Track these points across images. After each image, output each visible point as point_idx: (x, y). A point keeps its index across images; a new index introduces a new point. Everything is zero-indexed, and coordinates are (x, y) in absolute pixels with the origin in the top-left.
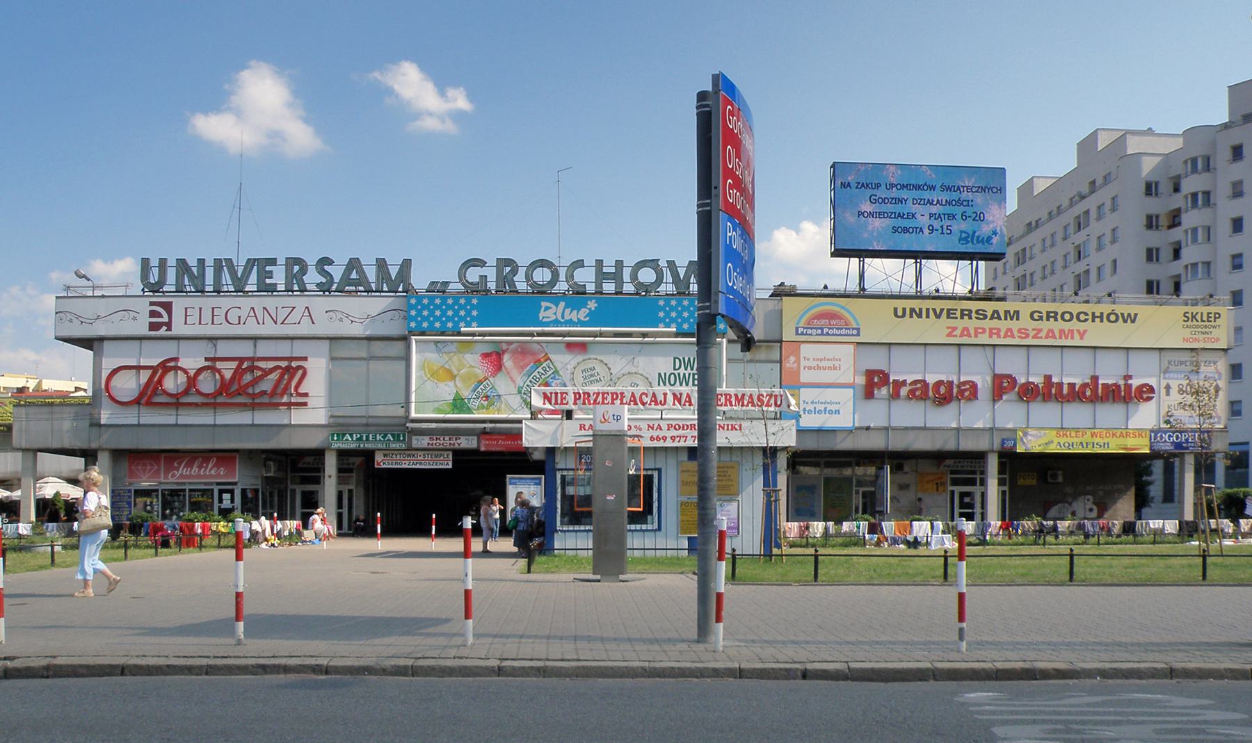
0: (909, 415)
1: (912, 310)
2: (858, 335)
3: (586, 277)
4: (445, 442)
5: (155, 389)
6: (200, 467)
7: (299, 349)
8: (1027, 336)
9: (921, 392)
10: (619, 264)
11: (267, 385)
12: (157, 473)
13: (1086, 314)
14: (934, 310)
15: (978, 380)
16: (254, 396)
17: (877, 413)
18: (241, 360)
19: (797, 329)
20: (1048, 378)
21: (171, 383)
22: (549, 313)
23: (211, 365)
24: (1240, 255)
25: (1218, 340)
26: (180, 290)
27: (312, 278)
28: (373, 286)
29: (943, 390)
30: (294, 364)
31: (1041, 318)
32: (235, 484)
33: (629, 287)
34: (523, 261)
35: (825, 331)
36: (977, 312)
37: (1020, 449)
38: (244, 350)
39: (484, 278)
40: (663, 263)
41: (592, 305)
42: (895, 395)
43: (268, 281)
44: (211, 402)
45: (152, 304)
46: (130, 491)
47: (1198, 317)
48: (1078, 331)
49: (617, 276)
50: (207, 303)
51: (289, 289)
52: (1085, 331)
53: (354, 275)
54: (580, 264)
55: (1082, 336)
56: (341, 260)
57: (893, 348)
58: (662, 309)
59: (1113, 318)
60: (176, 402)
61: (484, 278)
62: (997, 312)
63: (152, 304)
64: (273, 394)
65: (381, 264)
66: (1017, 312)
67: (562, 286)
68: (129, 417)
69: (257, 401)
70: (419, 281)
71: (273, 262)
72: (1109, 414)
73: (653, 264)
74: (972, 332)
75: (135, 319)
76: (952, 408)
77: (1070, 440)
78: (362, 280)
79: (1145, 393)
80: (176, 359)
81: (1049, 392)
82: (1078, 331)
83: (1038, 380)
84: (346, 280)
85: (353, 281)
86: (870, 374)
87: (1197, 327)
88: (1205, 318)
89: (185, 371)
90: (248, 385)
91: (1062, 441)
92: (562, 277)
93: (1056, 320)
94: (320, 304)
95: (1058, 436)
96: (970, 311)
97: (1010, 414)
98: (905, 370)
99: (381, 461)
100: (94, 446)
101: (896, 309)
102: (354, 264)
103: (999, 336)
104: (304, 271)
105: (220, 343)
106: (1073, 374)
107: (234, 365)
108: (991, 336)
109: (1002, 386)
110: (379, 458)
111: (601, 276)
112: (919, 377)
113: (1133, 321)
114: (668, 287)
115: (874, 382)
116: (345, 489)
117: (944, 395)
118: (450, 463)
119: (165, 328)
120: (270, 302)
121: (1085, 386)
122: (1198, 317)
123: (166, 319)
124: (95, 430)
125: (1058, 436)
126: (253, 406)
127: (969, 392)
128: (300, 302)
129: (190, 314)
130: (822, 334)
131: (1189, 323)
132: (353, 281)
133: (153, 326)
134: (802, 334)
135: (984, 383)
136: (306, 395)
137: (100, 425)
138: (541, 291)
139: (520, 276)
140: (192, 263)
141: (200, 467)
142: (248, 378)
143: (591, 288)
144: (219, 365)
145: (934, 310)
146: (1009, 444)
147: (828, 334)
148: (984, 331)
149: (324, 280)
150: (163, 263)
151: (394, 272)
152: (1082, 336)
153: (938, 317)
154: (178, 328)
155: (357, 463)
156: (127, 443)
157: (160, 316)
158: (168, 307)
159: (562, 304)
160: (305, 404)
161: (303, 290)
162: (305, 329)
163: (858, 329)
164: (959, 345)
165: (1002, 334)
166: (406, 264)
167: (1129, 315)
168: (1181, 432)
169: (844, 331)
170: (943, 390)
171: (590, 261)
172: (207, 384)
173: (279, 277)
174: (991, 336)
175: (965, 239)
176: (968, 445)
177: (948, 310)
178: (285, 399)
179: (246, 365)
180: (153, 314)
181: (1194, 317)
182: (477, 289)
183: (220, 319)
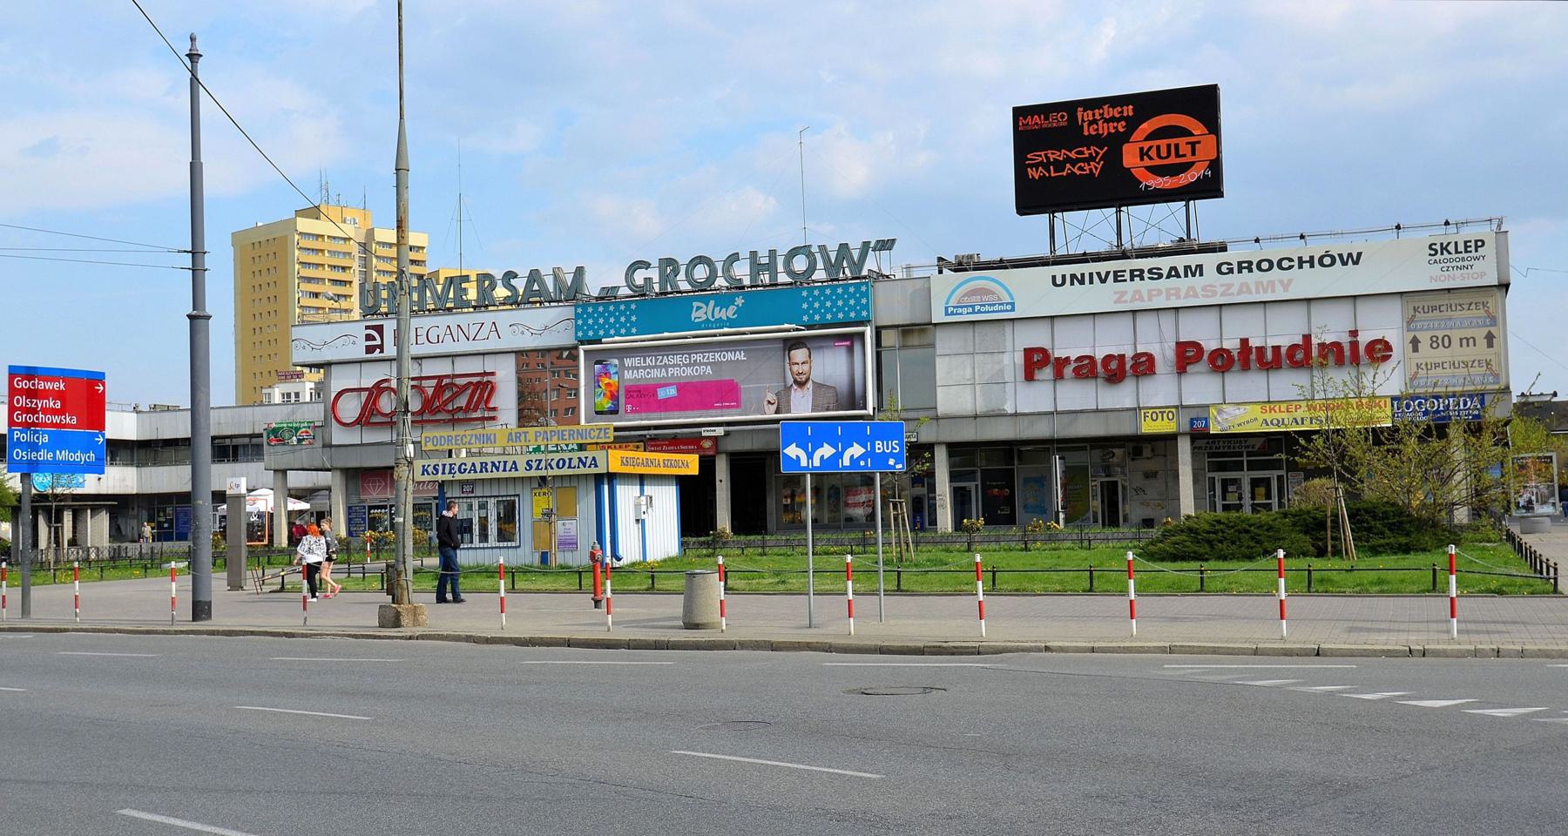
0: (1077, 395)
1: (1073, 276)
2: (1013, 310)
3: (742, 271)
5: (372, 410)
7: (489, 365)
8: (1214, 294)
9: (1086, 369)
11: (462, 401)
13: (1291, 260)
14: (1099, 274)
15: (1154, 350)
18: (440, 378)
20: (1245, 342)
22: (701, 313)
25: (1483, 274)
27: (501, 292)
29: (1113, 365)
31: (1231, 271)
33: (783, 278)
34: (683, 260)
36: (1150, 271)
38: (442, 368)
39: (648, 280)
40: (815, 249)
41: (739, 301)
42: (1059, 376)
45: (367, 328)
47: (1451, 248)
48: (1281, 282)
49: (771, 267)
52: (1290, 281)
53: (536, 287)
54: (734, 257)
55: (1286, 287)
56: (524, 272)
57: (1058, 324)
58: (805, 300)
59: (1327, 261)
62: (1174, 268)
63: (367, 328)
64: (467, 409)
65: (556, 275)
66: (1200, 267)
67: (721, 282)
68: (352, 437)
70: (593, 287)
71: (466, 279)
72: (1338, 380)
73: (805, 250)
74: (1145, 296)
77: (1279, 416)
79: (1379, 351)
81: (1248, 358)
82: (1281, 282)
83: (1232, 344)
85: (533, 295)
86: (1029, 353)
87: (1449, 260)
88: (1461, 248)
90: (446, 403)
91: (1268, 417)
93: (1251, 271)
94: (505, 317)
95: (1264, 411)
96: (1142, 271)
97: (1201, 388)
98: (1070, 345)
101: (1054, 277)
102: (534, 276)
103: (1178, 297)
104: (493, 286)
106: (1282, 332)
108: (1168, 298)
109: (1187, 355)
111: (756, 267)
112: (1087, 352)
113: (1356, 263)
114: (820, 274)
115: (1035, 361)
117: (1114, 371)
121: (1294, 347)
122: (1451, 248)
123: (378, 342)
125: (1264, 411)
127: (1144, 366)
131: (1438, 256)
132: (533, 295)
133: (370, 350)
135: (1164, 353)
136: (494, 409)
137: (331, 446)
138: (702, 288)
142: (447, 394)
143: (747, 282)
144: (425, 383)
145: (1099, 274)
146: (1200, 425)
147: (979, 312)
148: (1160, 292)
151: (569, 279)
152: (1286, 287)
153: (1103, 281)
158: (379, 329)
159: (712, 303)
160: (493, 418)
163: (1013, 304)
164: (1134, 312)
165: (1183, 293)
166: (580, 271)
167: (1350, 255)
168: (1437, 398)
169: (996, 308)
170: (1113, 365)
171: (745, 254)
174: (1168, 298)
176: (1149, 427)
178: (478, 414)
179: (443, 385)
180: (369, 337)
181: (1444, 248)
182: (641, 292)
183: (422, 339)
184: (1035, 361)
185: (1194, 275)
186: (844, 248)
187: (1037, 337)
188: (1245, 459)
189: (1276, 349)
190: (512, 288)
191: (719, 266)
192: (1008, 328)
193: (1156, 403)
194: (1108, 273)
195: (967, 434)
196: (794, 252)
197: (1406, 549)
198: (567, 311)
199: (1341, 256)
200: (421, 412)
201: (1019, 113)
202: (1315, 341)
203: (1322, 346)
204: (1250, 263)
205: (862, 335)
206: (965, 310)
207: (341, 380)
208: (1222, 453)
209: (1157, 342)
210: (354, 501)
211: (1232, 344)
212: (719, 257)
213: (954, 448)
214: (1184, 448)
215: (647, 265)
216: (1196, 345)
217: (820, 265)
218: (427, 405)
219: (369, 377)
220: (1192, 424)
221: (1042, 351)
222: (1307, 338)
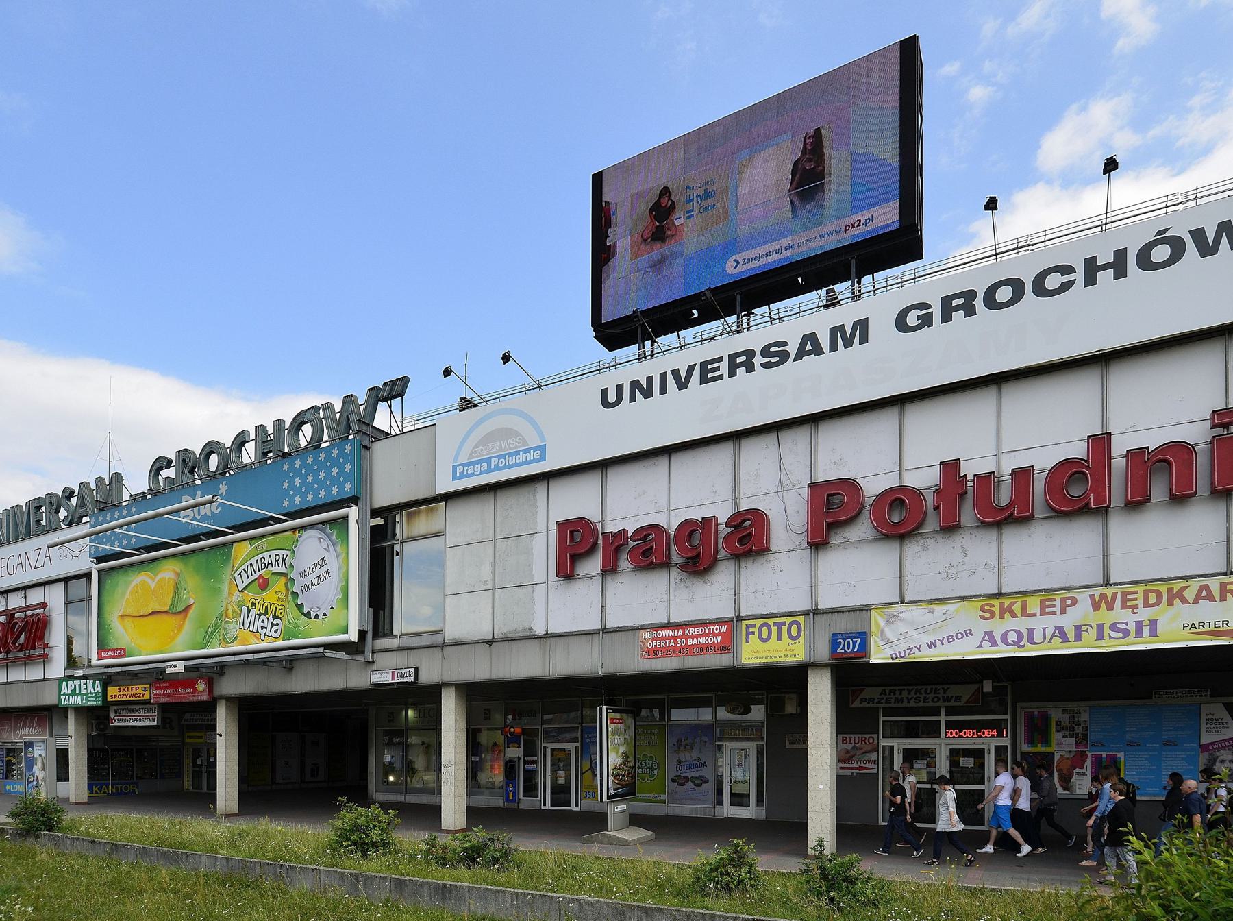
1: (635, 385)
2: (543, 458)
7: (35, 597)
9: (648, 550)
13: (1066, 269)
14: (676, 373)
15: (771, 508)
17: (576, 606)
19: (454, 468)
20: (949, 468)
24: (59, 779)
31: (926, 321)
35: (494, 462)
37: (878, 655)
42: (609, 570)
76: (723, 576)
77: (1023, 624)
83: (924, 478)
96: (750, 354)
97: (857, 572)
98: (627, 506)
101: (605, 392)
105: (30, 593)
109: (832, 509)
127: (747, 537)
130: (489, 470)
134: (462, 476)
135: (787, 516)
146: (849, 647)
147: (497, 468)
153: (682, 385)
163: (542, 448)
169: (520, 458)
176: (756, 652)
177: (704, 365)
184: (577, 545)
185: (848, 343)
187: (575, 501)
188: (943, 718)
189: (1023, 475)
192: (541, 489)
193: (769, 609)
194: (691, 369)
195: (480, 669)
197: (742, 805)
199: (1198, 235)
202: (1119, 447)
203: (1136, 455)
204: (970, 295)
206: (477, 469)
208: (882, 695)
209: (774, 485)
211: (924, 478)
213: (472, 692)
214: (820, 696)
215: (169, 464)
216: (850, 486)
220: (834, 644)
221: (583, 523)
222: (1100, 442)
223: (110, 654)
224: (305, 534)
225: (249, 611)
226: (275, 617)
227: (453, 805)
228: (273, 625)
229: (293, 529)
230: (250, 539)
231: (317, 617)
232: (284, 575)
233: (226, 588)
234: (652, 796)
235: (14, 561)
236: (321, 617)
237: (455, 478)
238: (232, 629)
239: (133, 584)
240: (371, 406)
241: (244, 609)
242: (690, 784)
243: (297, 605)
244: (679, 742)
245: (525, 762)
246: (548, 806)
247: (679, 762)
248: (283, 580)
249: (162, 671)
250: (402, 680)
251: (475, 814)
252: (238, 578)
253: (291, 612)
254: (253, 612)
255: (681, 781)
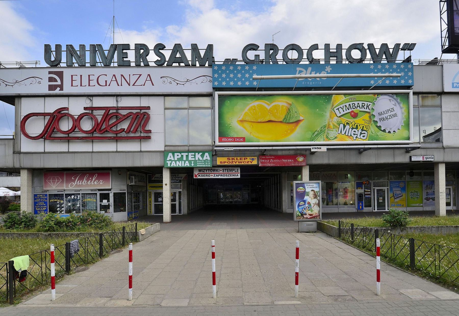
3: (319, 55)
4: (237, 161)
6: (88, 181)
7: (144, 102)
10: (339, 47)
12: (63, 182)
16: (117, 132)
18: (107, 109)
19: (453, 84)
21: (65, 125)
23: (90, 112)
26: (70, 65)
27: (152, 57)
28: (190, 63)
30: (143, 111)
32: (110, 190)
34: (281, 46)
38: (110, 103)
39: (257, 56)
43: (125, 59)
44: (90, 137)
45: (50, 73)
46: (46, 195)
50: (85, 72)
51: (138, 65)
53: (178, 55)
54: (315, 47)
56: (170, 46)
60: (68, 138)
61: (257, 56)
63: (50, 73)
64: (128, 131)
65: (195, 48)
68: (38, 146)
69: (119, 135)
71: (127, 47)
75: (40, 83)
78: (183, 59)
80: (67, 109)
84: (173, 59)
89: (72, 117)
92: (305, 56)
99: (197, 175)
100: (17, 166)
102: (178, 48)
105: (95, 99)
107: (102, 112)
110: (196, 172)
116: (177, 191)
118: (239, 175)
119: (58, 89)
120: (125, 71)
123: (59, 83)
124: (17, 156)
126: (117, 139)
128: (144, 71)
129: (75, 79)
133: (51, 88)
137: (20, 153)
139: (279, 56)
140: (77, 48)
141: (88, 181)
144: (95, 112)
149: (159, 59)
150: (58, 47)
151: (202, 53)
154: (67, 89)
155: (182, 175)
156: (38, 163)
157: (56, 81)
158: (60, 75)
161: (147, 65)
162: (148, 89)
166: (210, 47)
171: (321, 46)
172: (87, 125)
173: (131, 56)
175: (233, 170)
178: (138, 135)
180: (51, 79)
183: (94, 83)
186: (384, 46)
190: (162, 56)
191: (305, 52)
196: (354, 46)
198: (207, 71)
200: (92, 132)
201: (341, 45)
205: (408, 94)
207: (27, 107)
210: (38, 191)
212: (305, 46)
215: (253, 47)
217: (369, 56)
218: (97, 127)
219: (52, 106)
223: (226, 140)
224: (381, 97)
225: (344, 126)
226: (362, 130)
227: (443, 209)
228: (361, 133)
229: (374, 94)
230: (345, 94)
231: (389, 132)
232: (369, 113)
233: (328, 114)
234: (417, 205)
235: (109, 79)
236: (392, 132)
237: (453, 87)
238: (332, 133)
239: (251, 105)
240: (111, 52)
241: (342, 126)
242: (431, 200)
243: (377, 126)
244: (427, 186)
245: (365, 195)
246: (376, 210)
247: (427, 193)
248: (367, 115)
249: (310, 149)
250: (427, 160)
251: (448, 212)
252: (337, 112)
253: (373, 129)
254: (347, 127)
255: (427, 199)
